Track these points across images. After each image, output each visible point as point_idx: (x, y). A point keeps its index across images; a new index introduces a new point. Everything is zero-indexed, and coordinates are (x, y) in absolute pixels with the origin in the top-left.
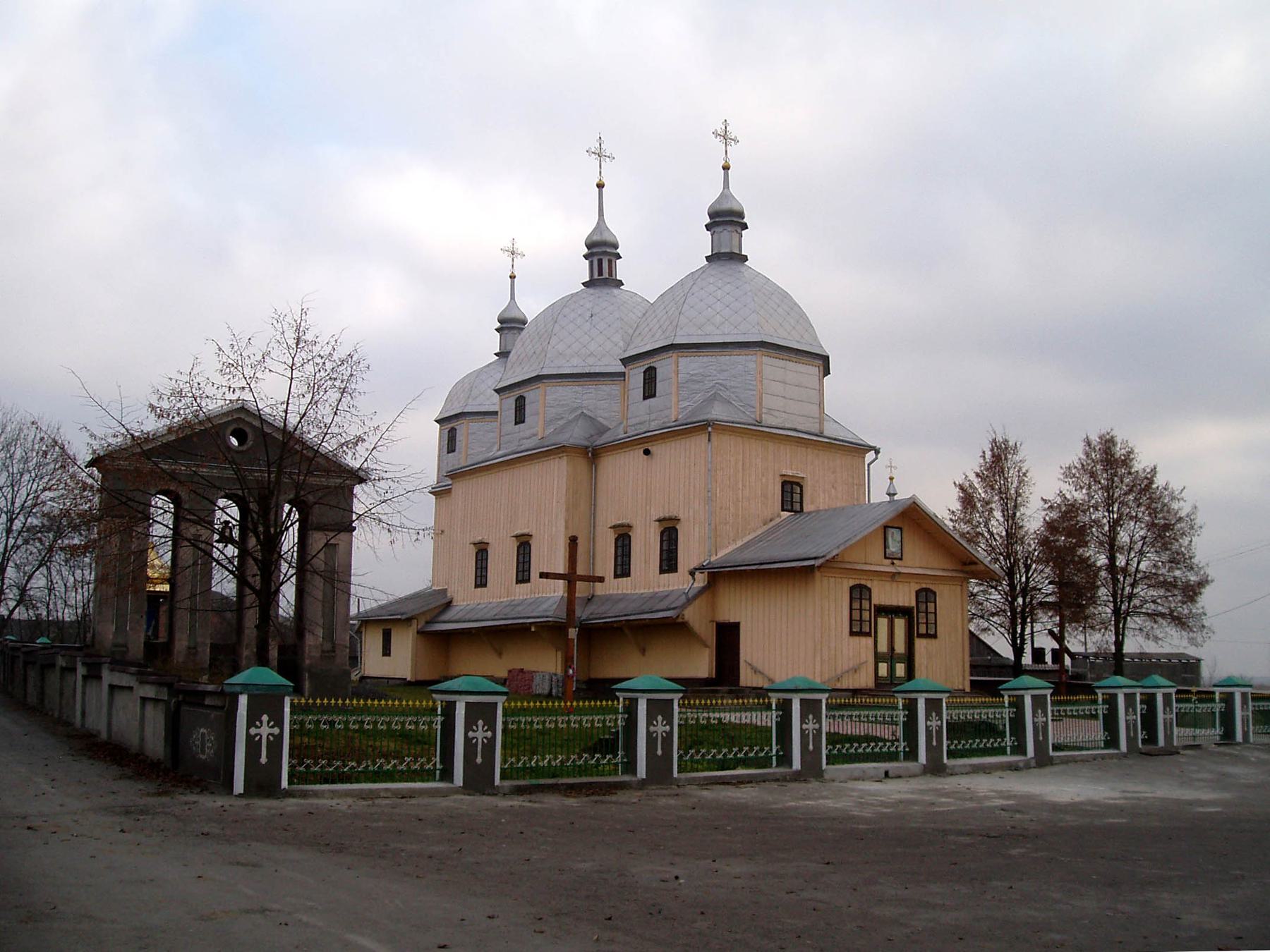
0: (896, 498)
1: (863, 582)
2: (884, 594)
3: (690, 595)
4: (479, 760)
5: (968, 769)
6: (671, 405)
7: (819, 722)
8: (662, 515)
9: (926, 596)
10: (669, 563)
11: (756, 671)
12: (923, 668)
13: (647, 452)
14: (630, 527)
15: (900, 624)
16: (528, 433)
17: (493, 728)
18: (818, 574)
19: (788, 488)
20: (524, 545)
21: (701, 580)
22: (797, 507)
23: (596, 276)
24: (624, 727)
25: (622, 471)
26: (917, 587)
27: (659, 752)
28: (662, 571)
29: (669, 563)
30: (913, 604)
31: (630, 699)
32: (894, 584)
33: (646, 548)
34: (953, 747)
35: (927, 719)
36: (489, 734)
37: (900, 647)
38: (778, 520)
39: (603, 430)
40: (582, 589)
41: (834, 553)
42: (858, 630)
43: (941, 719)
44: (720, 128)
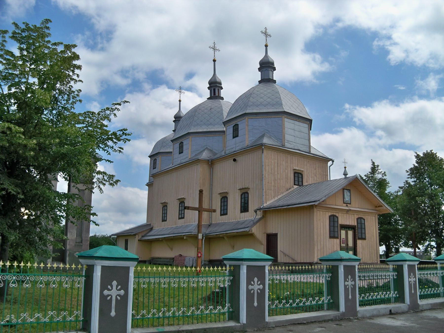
0: (347, 176)
1: (335, 214)
2: (343, 220)
3: (255, 221)
4: (113, 313)
5: (430, 307)
6: (246, 138)
7: (354, 280)
8: (241, 187)
9: (360, 220)
10: (245, 208)
11: (285, 255)
12: (361, 253)
13: (235, 160)
14: (227, 193)
15: (350, 233)
16: (184, 157)
17: (125, 287)
18: (315, 210)
19: (296, 175)
20: (182, 202)
21: (260, 215)
22: (300, 183)
23: (213, 95)
24: (230, 286)
25: (224, 170)
26: (357, 217)
27: (256, 304)
28: (242, 212)
29: (245, 208)
30: (356, 224)
31: (234, 266)
32: (348, 215)
33: (234, 203)
34: (422, 293)
35: (409, 277)
36: (122, 292)
37: (351, 244)
38: (292, 189)
39: (215, 154)
40: (205, 215)
41: (323, 199)
42: (333, 235)
43: (415, 277)
44: (264, 30)
